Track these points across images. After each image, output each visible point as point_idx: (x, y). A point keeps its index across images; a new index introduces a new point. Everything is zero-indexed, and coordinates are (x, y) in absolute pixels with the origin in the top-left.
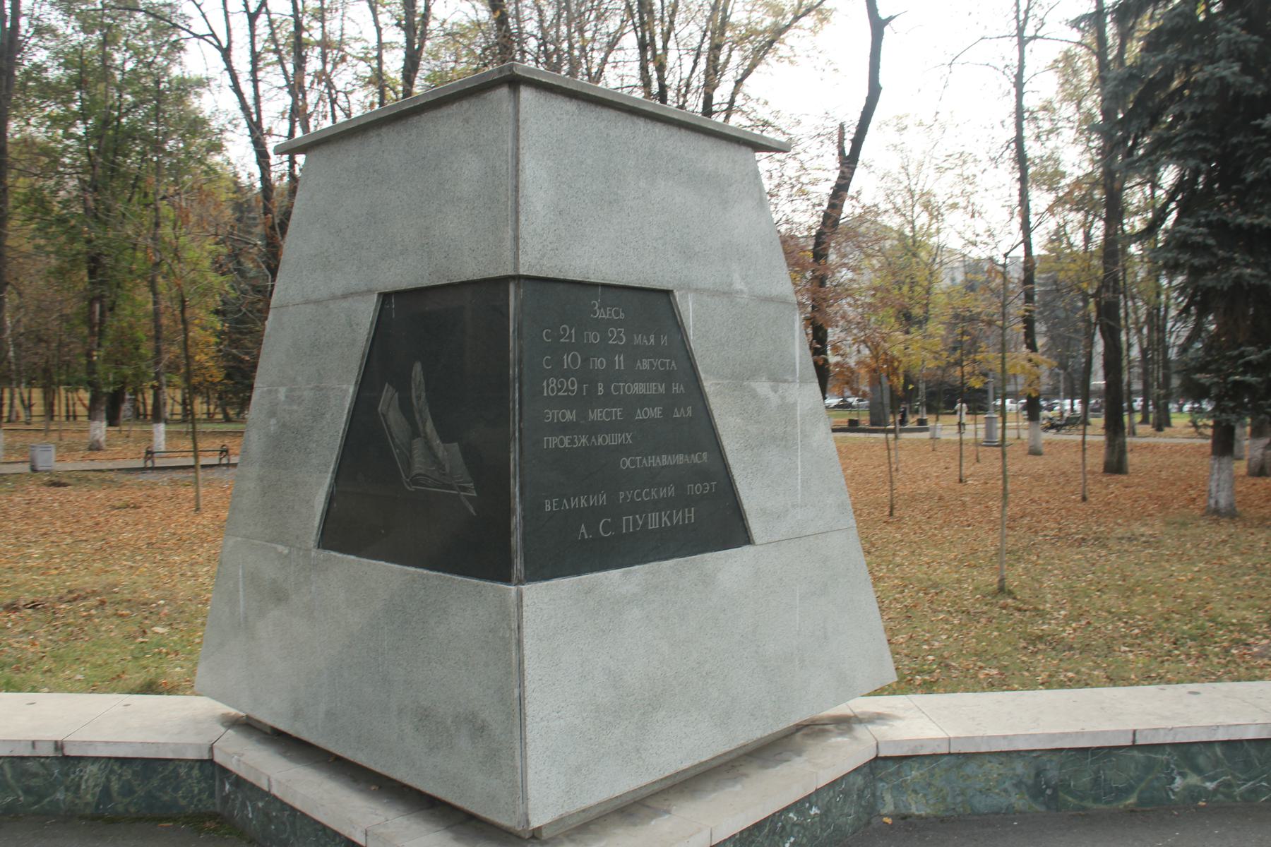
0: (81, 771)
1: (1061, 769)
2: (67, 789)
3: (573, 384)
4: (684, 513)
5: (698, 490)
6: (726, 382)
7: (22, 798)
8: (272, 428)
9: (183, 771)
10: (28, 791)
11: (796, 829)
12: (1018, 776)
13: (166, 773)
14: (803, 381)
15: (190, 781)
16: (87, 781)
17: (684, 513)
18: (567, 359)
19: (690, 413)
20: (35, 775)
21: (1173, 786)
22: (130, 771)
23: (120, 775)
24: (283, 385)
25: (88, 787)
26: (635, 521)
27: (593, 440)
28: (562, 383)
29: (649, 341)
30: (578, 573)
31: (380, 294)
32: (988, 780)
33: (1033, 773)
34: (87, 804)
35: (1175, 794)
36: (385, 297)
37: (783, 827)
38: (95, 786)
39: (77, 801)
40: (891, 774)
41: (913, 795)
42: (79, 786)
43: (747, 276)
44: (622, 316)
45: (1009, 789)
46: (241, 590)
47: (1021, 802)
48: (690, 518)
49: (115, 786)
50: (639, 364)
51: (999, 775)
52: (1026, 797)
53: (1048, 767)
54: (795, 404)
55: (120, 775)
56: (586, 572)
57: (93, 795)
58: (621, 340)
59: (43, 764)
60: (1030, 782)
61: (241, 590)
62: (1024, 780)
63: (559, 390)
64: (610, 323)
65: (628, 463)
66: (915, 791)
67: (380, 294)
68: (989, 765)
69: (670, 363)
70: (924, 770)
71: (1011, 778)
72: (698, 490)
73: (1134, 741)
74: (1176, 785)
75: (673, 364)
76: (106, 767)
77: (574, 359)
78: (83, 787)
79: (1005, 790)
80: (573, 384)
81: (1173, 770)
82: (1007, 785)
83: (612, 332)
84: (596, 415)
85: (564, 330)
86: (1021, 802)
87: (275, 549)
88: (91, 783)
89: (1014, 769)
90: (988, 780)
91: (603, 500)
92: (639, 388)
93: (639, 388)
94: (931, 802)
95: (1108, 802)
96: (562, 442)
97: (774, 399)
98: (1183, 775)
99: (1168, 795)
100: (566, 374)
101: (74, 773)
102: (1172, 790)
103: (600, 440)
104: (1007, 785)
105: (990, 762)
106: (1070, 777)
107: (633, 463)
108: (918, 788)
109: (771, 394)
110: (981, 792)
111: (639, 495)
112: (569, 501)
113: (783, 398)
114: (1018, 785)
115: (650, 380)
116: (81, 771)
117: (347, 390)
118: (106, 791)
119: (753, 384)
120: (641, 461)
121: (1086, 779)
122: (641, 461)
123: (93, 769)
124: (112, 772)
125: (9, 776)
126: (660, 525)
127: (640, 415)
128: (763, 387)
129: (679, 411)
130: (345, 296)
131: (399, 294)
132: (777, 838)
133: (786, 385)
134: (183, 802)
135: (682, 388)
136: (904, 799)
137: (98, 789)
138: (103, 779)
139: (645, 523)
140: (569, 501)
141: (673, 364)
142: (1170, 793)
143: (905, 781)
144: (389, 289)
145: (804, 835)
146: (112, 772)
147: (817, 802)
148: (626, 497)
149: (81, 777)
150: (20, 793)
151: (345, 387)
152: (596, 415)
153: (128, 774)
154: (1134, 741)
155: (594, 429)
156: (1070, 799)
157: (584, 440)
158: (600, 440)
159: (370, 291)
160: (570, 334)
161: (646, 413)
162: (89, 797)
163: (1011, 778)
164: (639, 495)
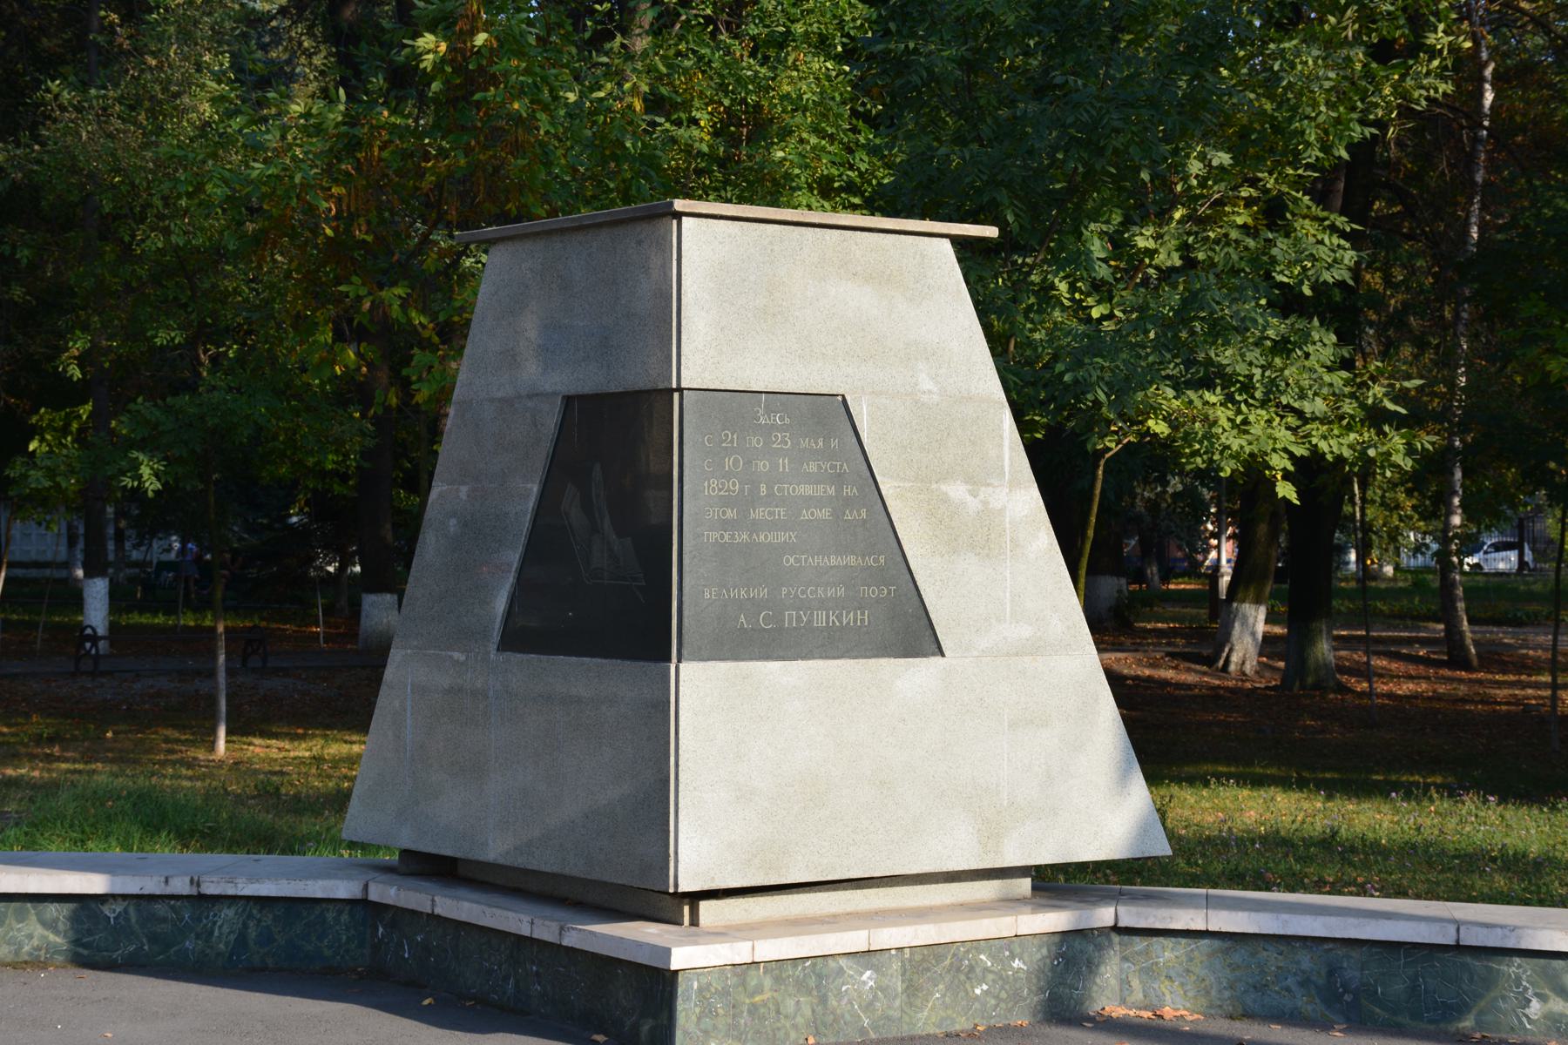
0: (215, 915)
1: (1362, 970)
2: (198, 937)
3: (734, 485)
4: (855, 614)
5: (873, 593)
6: (908, 485)
7: (146, 947)
8: (452, 529)
9: (330, 916)
10: (153, 938)
11: (990, 977)
12: (1304, 972)
13: (313, 917)
14: (1014, 484)
15: (337, 928)
16: (220, 927)
17: (855, 614)
18: (729, 462)
19: (864, 515)
20: (164, 920)
21: (1527, 1011)
22: (271, 916)
23: (259, 921)
24: (464, 483)
25: (221, 934)
26: (799, 618)
27: (755, 536)
28: (723, 484)
29: (816, 443)
30: (736, 657)
31: (564, 397)
32: (1263, 972)
33: (1323, 972)
34: (218, 954)
35: (1530, 1021)
36: (569, 400)
37: (971, 968)
38: (229, 933)
39: (208, 951)
40: (1139, 953)
41: (1167, 983)
42: (212, 933)
43: (937, 375)
44: (787, 421)
45: (1294, 988)
46: (409, 708)
47: (1310, 1008)
48: (862, 621)
49: (252, 933)
50: (805, 466)
51: (1278, 968)
52: (1318, 1001)
53: (1345, 965)
54: (1002, 511)
55: (259, 921)
56: (743, 660)
57: (227, 944)
58: (786, 443)
59: (172, 908)
60: (1321, 982)
61: (409, 708)
62: (1314, 978)
63: (720, 490)
64: (773, 427)
65: (792, 560)
66: (1169, 978)
67: (564, 397)
68: (1265, 953)
69: (842, 466)
70: (1181, 951)
71: (1295, 974)
72: (873, 593)
73: (1458, 941)
74: (1532, 1010)
75: (845, 467)
76: (244, 910)
77: (736, 462)
78: (216, 933)
79: (1288, 989)
80: (734, 485)
81: (1526, 989)
82: (1290, 981)
83: (776, 436)
84: (760, 513)
85: (727, 435)
86: (1310, 1008)
87: (450, 657)
88: (226, 929)
89: (1298, 963)
90: (1263, 972)
91: (764, 593)
92: (806, 490)
93: (806, 490)
94: (1190, 994)
95: (1431, 1022)
96: (722, 537)
97: (973, 504)
98: (1543, 998)
99: (1521, 1023)
100: (727, 476)
101: (207, 917)
102: (1527, 1016)
103: (762, 537)
104: (1290, 981)
105: (1264, 949)
106: (1375, 981)
107: (798, 560)
108: (1172, 974)
109: (969, 498)
110: (1255, 987)
111: (803, 592)
112: (728, 591)
113: (985, 503)
114: (1305, 983)
115: (818, 482)
116: (215, 915)
117: (531, 489)
118: (242, 939)
119: (944, 487)
120: (806, 560)
121: (1399, 987)
122: (806, 560)
123: (228, 913)
124: (250, 916)
125: (133, 920)
126: (827, 623)
127: (806, 515)
128: (957, 491)
129: (851, 512)
130: (530, 397)
131: (582, 398)
132: (963, 977)
133: (990, 489)
134: (327, 953)
135: (855, 490)
136: (1156, 986)
137: (232, 937)
138: (240, 925)
139: (810, 621)
140: (728, 591)
141: (845, 467)
142: (1524, 1020)
143: (1157, 963)
144: (572, 392)
145: (1002, 988)
146: (250, 916)
147: (1022, 954)
148: (789, 593)
149: (215, 923)
150: (144, 940)
151: (529, 486)
152: (760, 513)
153: (268, 919)
154: (1458, 941)
155: (755, 527)
156: (1378, 1010)
157: (745, 537)
158: (762, 537)
159: (555, 394)
160: (733, 439)
161: (813, 514)
162: (222, 946)
163: (1295, 974)
164: (803, 592)
